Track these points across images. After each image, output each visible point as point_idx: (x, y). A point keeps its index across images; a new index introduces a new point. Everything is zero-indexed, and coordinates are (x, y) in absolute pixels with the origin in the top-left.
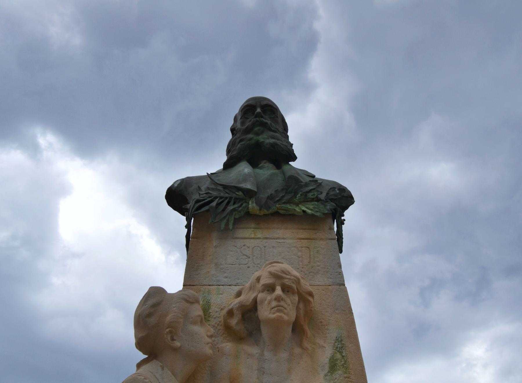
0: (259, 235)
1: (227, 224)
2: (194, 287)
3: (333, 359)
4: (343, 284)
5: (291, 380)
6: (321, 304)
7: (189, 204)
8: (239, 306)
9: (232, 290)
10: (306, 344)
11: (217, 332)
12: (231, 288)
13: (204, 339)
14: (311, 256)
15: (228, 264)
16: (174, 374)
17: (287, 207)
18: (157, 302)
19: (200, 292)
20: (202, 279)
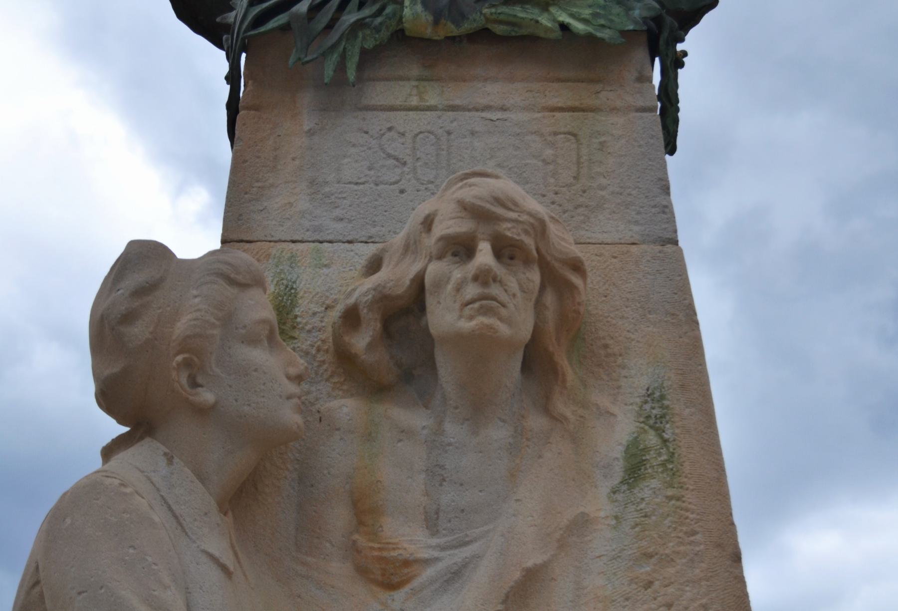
0: (432, 99)
1: (341, 67)
2: (252, 245)
3: (637, 448)
4: (670, 239)
5: (517, 500)
6: (606, 296)
7: (234, 11)
8: (374, 296)
9: (357, 254)
10: (561, 406)
11: (315, 369)
12: (353, 248)
13: (280, 385)
14: (582, 160)
15: (345, 184)
16: (202, 478)
17: (515, 13)
18: (147, 283)
19: (268, 260)
20: (274, 222)
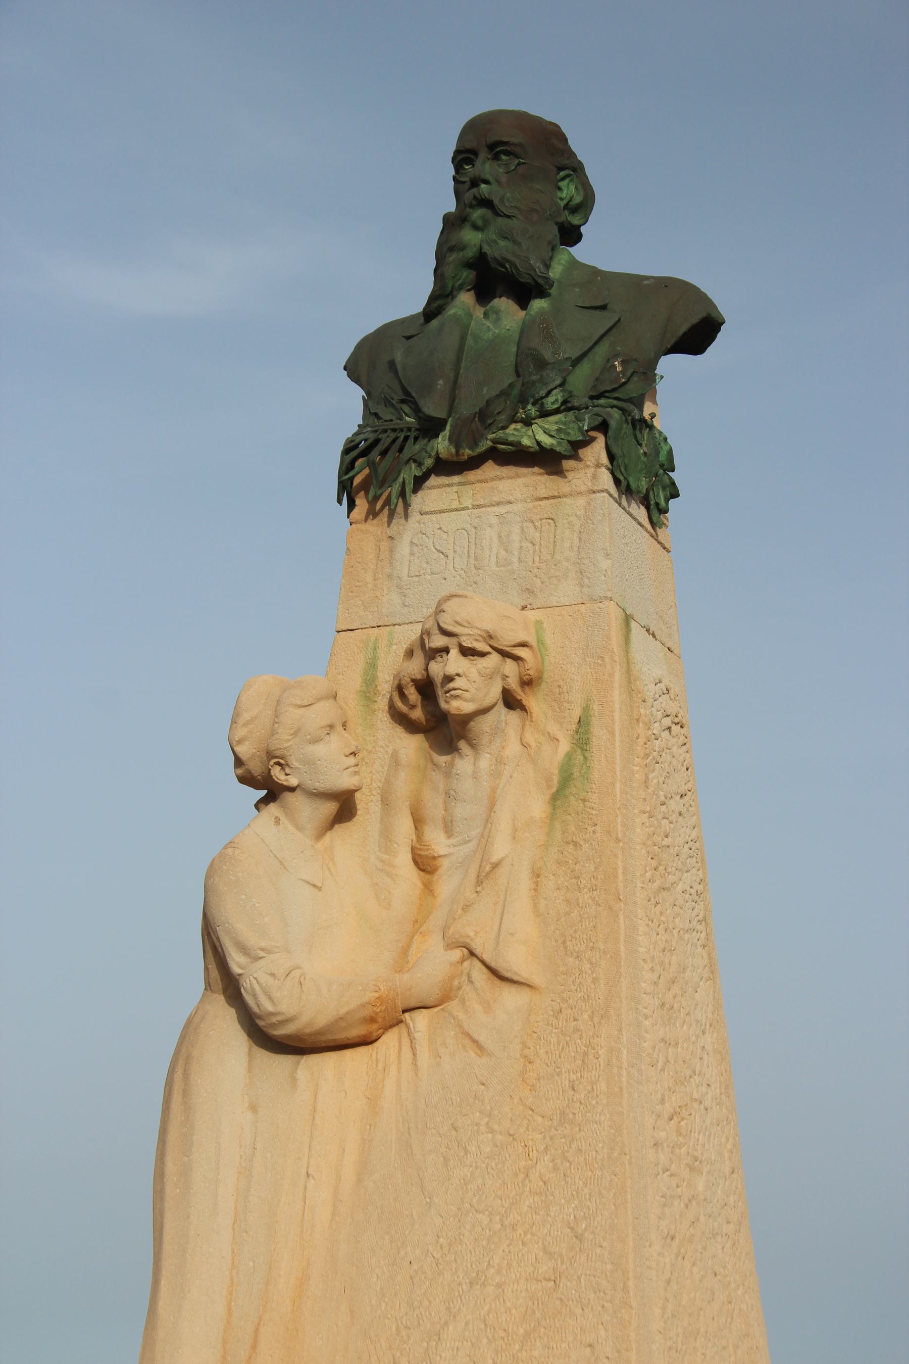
16: (300, 828)
